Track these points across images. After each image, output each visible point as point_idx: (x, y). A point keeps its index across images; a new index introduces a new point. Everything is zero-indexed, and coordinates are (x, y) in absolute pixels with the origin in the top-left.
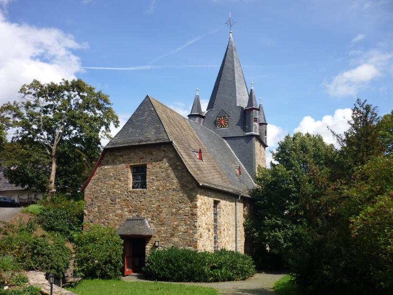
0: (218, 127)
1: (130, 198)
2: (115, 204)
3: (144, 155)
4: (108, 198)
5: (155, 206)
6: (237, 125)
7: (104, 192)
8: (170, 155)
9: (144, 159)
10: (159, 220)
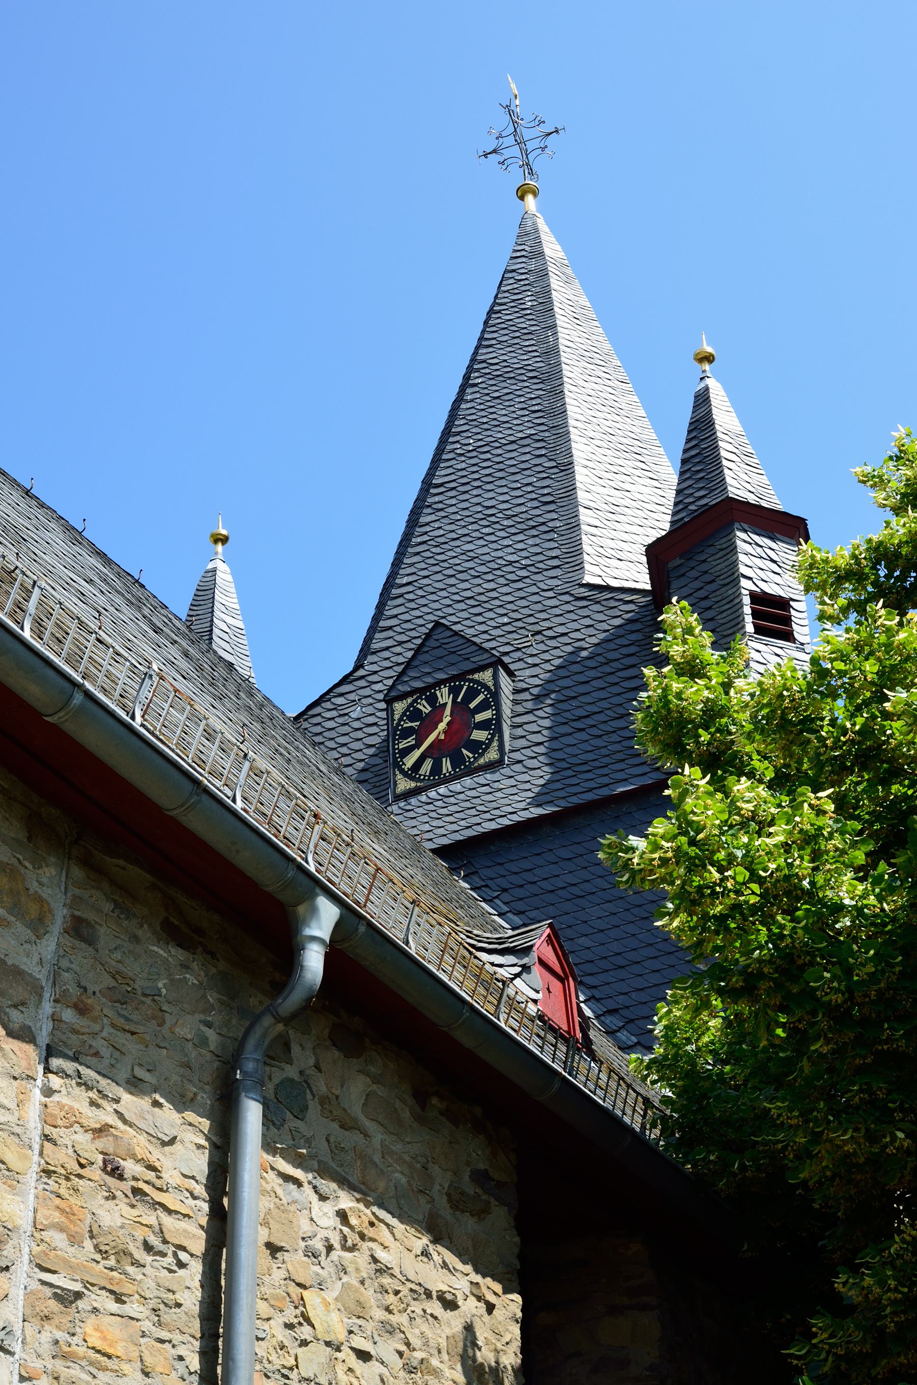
0: (404, 784)
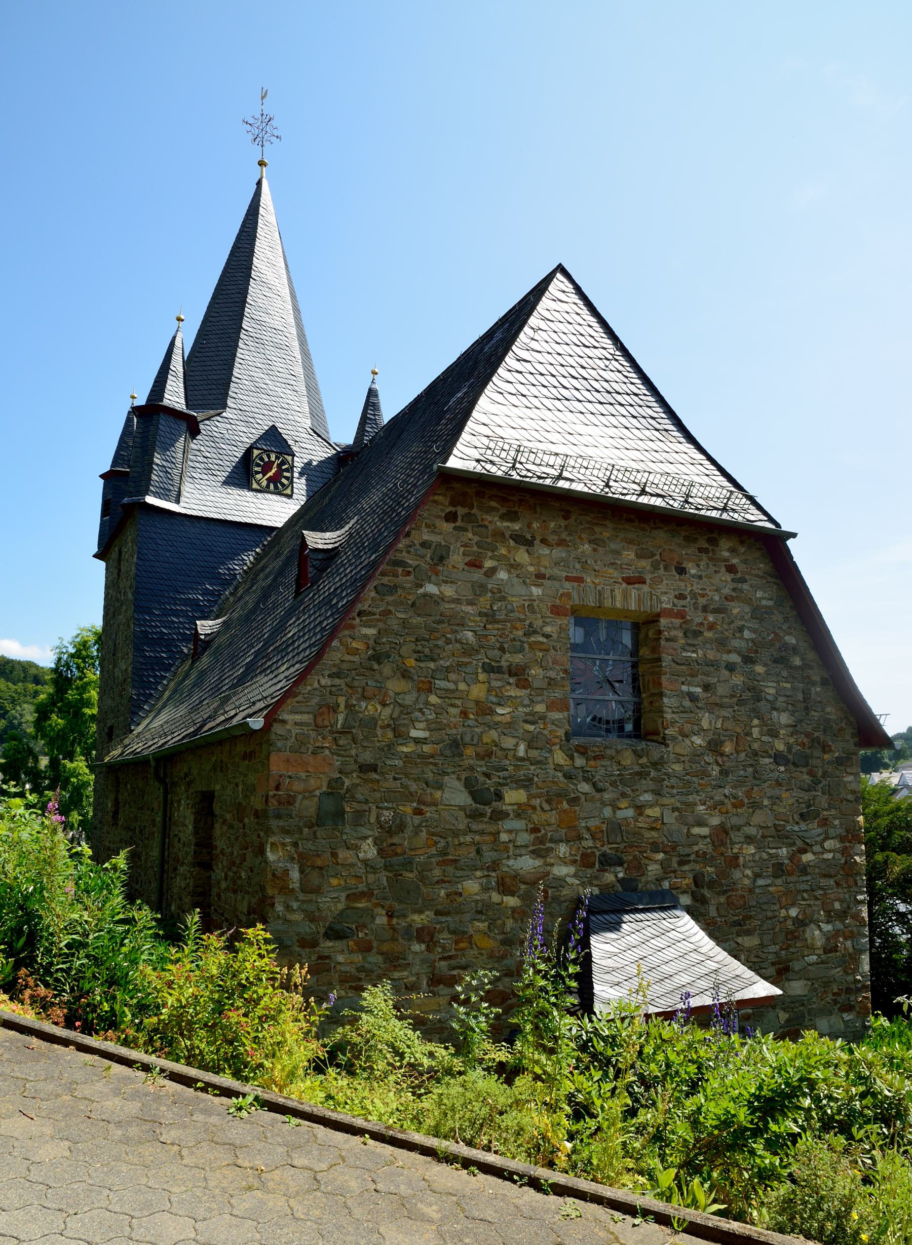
1: (585, 787)
2: (499, 816)
3: (645, 564)
4: (451, 781)
5: (704, 831)
6: (102, 476)
7: (417, 741)
8: (759, 594)
9: (646, 588)
10: (729, 903)
